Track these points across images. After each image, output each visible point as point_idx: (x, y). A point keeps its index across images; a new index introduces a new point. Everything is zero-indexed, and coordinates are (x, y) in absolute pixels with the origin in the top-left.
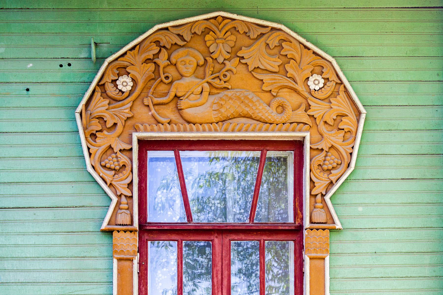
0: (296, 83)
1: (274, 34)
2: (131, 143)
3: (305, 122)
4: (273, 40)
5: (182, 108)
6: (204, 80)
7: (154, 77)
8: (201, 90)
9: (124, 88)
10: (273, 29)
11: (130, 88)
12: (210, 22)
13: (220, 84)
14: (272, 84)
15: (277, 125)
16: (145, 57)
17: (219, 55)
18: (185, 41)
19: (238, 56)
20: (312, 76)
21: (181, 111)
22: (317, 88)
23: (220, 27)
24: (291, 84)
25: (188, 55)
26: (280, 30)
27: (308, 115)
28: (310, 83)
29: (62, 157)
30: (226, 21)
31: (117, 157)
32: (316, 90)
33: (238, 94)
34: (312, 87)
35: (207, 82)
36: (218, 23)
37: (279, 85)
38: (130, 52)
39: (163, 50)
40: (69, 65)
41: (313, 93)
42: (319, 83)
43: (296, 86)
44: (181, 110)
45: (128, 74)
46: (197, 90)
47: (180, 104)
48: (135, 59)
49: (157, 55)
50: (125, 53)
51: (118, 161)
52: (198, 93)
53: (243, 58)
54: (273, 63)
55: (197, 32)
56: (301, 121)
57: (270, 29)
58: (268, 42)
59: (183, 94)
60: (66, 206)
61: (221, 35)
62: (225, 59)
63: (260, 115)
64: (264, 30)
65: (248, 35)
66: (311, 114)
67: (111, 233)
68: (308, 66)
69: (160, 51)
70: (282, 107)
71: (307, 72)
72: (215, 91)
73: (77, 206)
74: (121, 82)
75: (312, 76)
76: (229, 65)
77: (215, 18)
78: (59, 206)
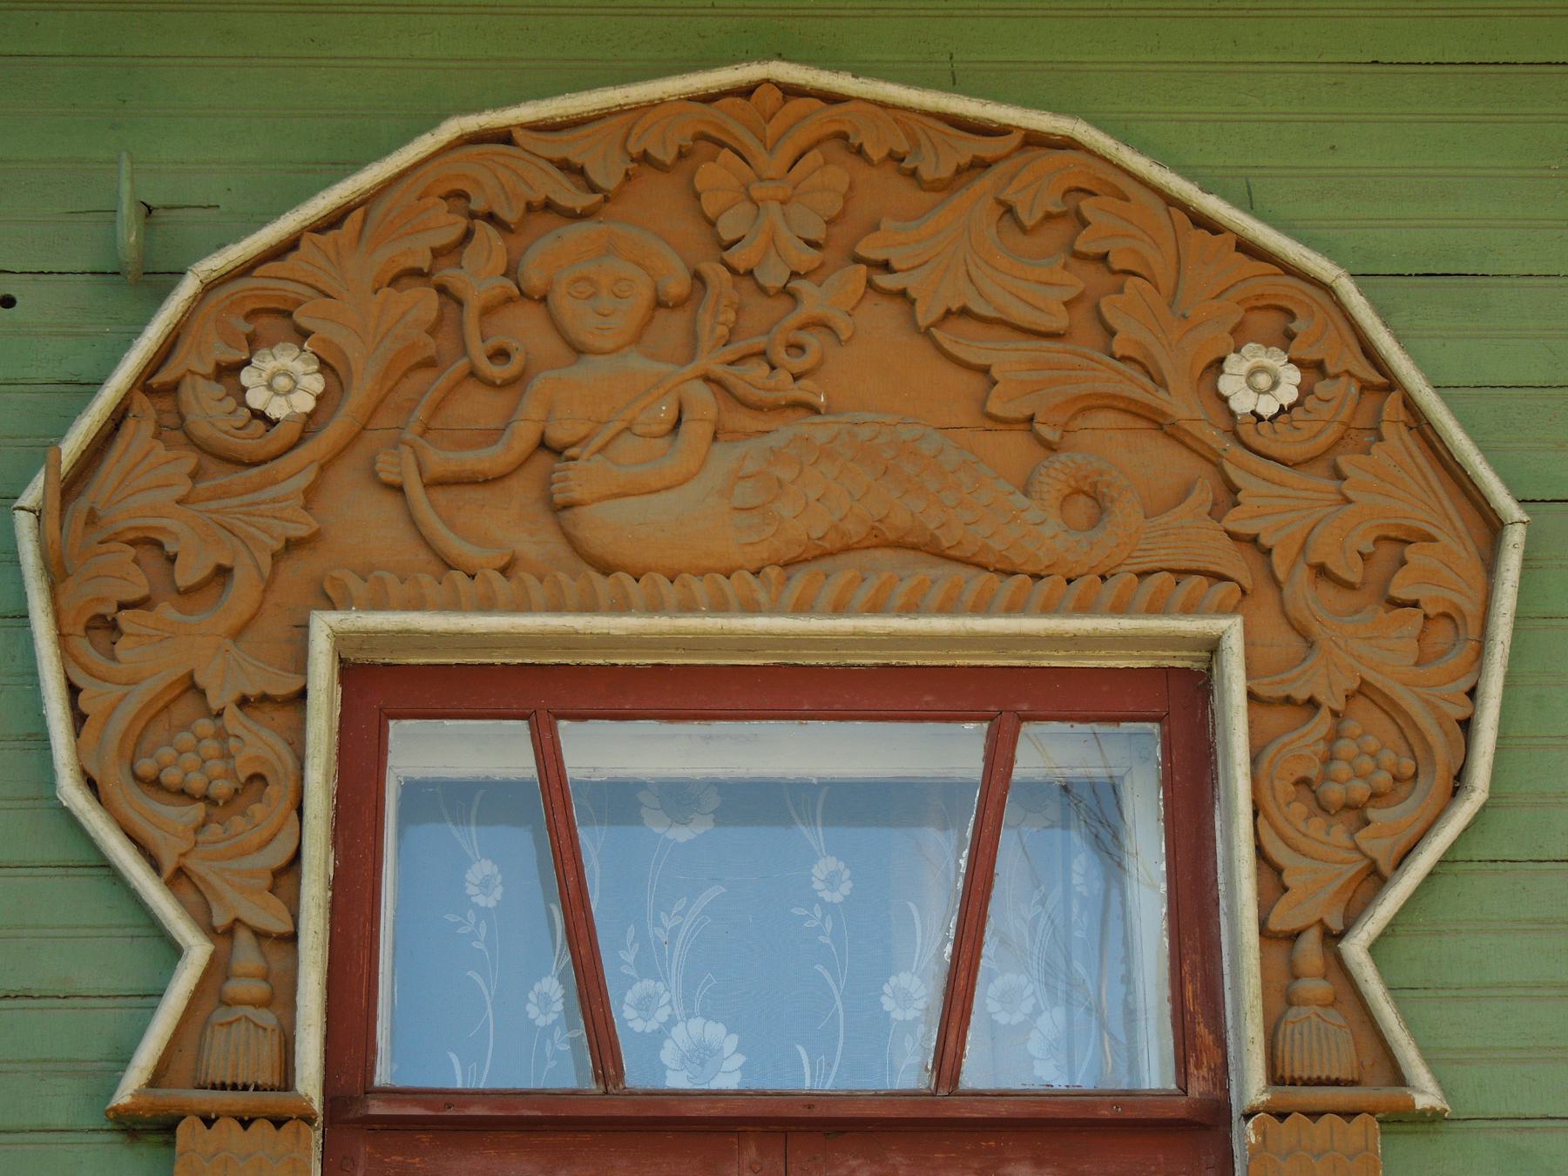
0: (1162, 384)
4: (1035, 190)
5: (577, 494)
6: (689, 370)
9: (281, 401)
10: (1034, 140)
18: (593, 188)
19: (858, 260)
20: (1237, 351)
21: (566, 514)
22: (1268, 407)
24: (1135, 387)
26: (1069, 144)
27: (1226, 531)
30: (798, 105)
31: (222, 735)
32: (1260, 418)
34: (1242, 403)
35: (707, 379)
37: (1084, 389)
41: (1247, 431)
42: (1275, 384)
43: (1159, 399)
44: (567, 506)
50: (289, 246)
51: (226, 755)
52: (656, 429)
53: (886, 266)
54: (1035, 287)
55: (656, 152)
56: (1194, 565)
57: (1014, 140)
58: (1009, 195)
59: (582, 430)
61: (773, 164)
66: (1247, 528)
69: (468, 235)
72: (745, 420)
75: (1237, 351)
77: (746, 91)
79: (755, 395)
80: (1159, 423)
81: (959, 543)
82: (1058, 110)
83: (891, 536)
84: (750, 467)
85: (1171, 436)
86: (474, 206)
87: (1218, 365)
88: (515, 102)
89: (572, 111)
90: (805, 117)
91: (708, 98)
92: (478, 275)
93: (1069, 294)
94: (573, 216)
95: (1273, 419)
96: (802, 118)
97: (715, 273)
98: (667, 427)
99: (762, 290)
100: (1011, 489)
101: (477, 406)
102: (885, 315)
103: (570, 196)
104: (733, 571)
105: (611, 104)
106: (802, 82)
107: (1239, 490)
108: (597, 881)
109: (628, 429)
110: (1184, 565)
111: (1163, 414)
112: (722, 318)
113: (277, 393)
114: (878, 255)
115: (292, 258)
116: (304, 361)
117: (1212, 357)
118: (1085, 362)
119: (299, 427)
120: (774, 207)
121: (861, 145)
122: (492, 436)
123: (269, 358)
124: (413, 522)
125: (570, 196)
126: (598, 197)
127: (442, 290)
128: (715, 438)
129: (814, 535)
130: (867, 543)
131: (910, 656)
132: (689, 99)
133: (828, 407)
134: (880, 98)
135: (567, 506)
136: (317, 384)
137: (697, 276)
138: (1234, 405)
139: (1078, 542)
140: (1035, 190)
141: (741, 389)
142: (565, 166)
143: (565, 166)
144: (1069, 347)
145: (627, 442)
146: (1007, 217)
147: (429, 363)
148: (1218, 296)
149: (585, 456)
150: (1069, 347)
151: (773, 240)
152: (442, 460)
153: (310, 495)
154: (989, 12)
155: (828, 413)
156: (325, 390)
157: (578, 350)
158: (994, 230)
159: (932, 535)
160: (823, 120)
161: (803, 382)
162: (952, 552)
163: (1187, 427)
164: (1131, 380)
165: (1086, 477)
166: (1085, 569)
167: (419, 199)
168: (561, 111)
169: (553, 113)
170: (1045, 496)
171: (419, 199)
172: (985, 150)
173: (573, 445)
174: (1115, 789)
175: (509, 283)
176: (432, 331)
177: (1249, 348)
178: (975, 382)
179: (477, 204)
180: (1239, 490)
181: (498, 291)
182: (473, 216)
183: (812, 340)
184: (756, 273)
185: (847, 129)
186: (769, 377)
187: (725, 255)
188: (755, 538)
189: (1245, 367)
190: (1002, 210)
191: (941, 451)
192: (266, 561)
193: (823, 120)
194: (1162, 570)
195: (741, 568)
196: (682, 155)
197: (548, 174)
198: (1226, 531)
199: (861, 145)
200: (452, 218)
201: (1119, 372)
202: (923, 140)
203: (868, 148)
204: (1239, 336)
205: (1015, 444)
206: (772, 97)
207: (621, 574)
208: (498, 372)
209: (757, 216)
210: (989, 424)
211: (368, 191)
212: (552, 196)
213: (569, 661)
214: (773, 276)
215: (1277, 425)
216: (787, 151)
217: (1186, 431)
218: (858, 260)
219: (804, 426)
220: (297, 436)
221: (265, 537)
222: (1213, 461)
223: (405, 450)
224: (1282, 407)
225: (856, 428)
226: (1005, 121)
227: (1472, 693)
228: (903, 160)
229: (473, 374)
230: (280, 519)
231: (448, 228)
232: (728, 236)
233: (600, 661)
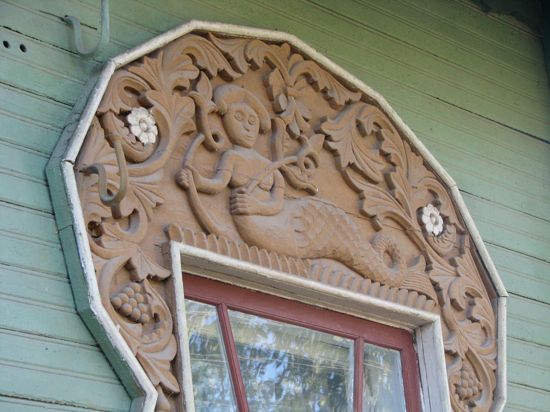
2: (167, 263)
5: (248, 210)
10: (366, 99)
21: (240, 217)
26: (375, 103)
29: (20, 266)
31: (144, 291)
35: (281, 170)
38: (149, 59)
40: (23, 48)
41: (430, 239)
44: (241, 214)
47: (243, 202)
50: (139, 61)
51: (146, 302)
60: (36, 396)
63: (366, 261)
66: (436, 279)
73: (59, 399)
78: (21, 392)
82: (376, 89)
85: (407, 235)
108: (505, 366)
110: (421, 291)
111: (410, 226)
131: (334, 307)
132: (261, 40)
135: (241, 214)
143: (226, 56)
159: (352, 258)
162: (356, 267)
165: (391, 246)
170: (381, 251)
174: (131, 398)
185: (311, 73)
206: (286, 49)
210: (360, 216)
213: (231, 283)
217: (416, 235)
227: (496, 360)
233: (241, 286)
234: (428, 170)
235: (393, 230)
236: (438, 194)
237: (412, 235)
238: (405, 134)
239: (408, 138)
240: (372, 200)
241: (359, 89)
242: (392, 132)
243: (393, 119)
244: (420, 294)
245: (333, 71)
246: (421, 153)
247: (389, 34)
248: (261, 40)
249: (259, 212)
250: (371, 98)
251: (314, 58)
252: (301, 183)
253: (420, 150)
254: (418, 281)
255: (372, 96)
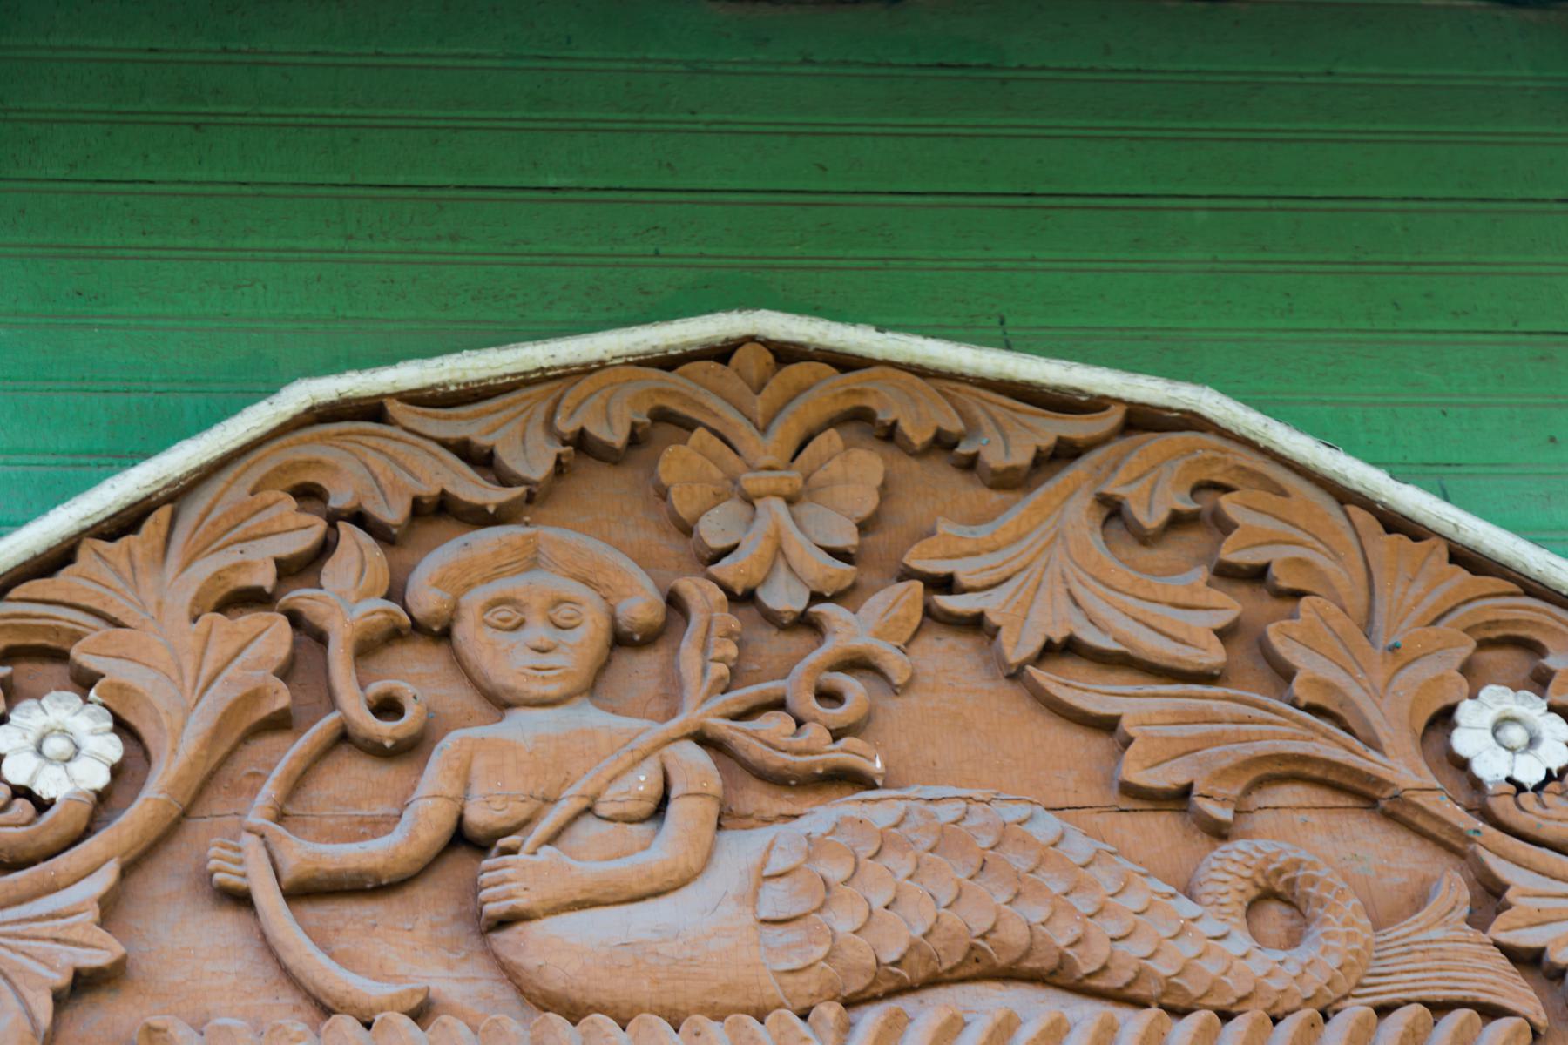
0: (1373, 743)
1: (1133, 458)
3: (1484, 998)
4: (1154, 483)
6: (673, 726)
7: (282, 700)
8: (657, 789)
9: (55, 772)
10: (1142, 420)
11: (101, 779)
12: (684, 375)
13: (801, 742)
14: (1190, 750)
15: (1226, 1016)
16: (218, 576)
17: (772, 567)
18: (505, 480)
19: (907, 574)
20: (1473, 695)
22: (1530, 773)
23: (760, 405)
24: (1329, 747)
25: (532, 561)
26: (1192, 422)
27: (1497, 945)
28: (1470, 738)
30: (797, 372)
32: (1521, 788)
33: (947, 813)
34: (1491, 766)
35: (703, 739)
36: (749, 383)
37: (1247, 751)
38: (102, 545)
39: (351, 537)
41: (1503, 807)
42: (1533, 742)
43: (1371, 762)
44: (504, 922)
45: (84, 682)
46: (621, 786)
48: (136, 586)
49: (302, 568)
52: (632, 808)
53: (946, 584)
54: (1179, 612)
55: (599, 431)
56: (1457, 995)
57: (1115, 416)
58: (1113, 488)
59: (521, 811)
61: (770, 447)
62: (816, 597)
64: (1077, 428)
65: (964, 449)
66: (1527, 938)
67: (351, 731)
68: (1432, 631)
69: (325, 548)
70: (1268, 895)
71: (1436, 670)
72: (757, 799)
74: (32, 738)
75: (1473, 695)
76: (848, 629)
77: (722, 353)
79: (778, 760)
80: (1363, 794)
81: (1105, 968)
83: (1002, 960)
84: (778, 863)
85: (1390, 817)
86: (334, 503)
87: (1445, 718)
88: (391, 360)
89: (473, 375)
90: (807, 389)
91: (668, 362)
92: (347, 597)
93: (1222, 619)
94: (480, 518)
95: (1538, 788)
96: (802, 389)
97: (701, 594)
98: (649, 806)
99: (771, 618)
100: (1172, 890)
101: (353, 780)
102: (945, 656)
103: (473, 489)
104: (767, 1013)
105: (529, 366)
106: (803, 339)
107: (1505, 887)
109: (589, 810)
110: (1441, 994)
111: (1380, 782)
112: (718, 653)
113: (50, 760)
114: (940, 567)
115: (65, 576)
116: (92, 716)
117: (1438, 704)
118: (1258, 713)
119: (86, 808)
120: (779, 505)
121: (895, 424)
122: (380, 826)
123: (38, 712)
124: (268, 948)
125: (473, 489)
126: (518, 491)
127: (295, 619)
128: (719, 826)
129: (890, 956)
130: (962, 972)
132: (639, 364)
133: (885, 776)
134: (918, 361)
135: (504, 922)
136: (114, 749)
137: (675, 603)
138: (1480, 769)
139: (1282, 963)
140: (1154, 483)
141: (756, 752)
142: (465, 451)
143: (465, 451)
144: (1231, 692)
145: (589, 829)
146: (1116, 525)
147: (281, 723)
148: (1435, 622)
149: (529, 844)
150: (1231, 692)
151: (779, 550)
152: (308, 854)
153: (110, 909)
154: (1048, 265)
155: (885, 787)
156: (124, 758)
157: (500, 703)
158: (1100, 538)
160: (831, 392)
161: (844, 742)
163: (1418, 800)
164: (1327, 736)
165: (1279, 872)
166: (1297, 1002)
167: (253, 493)
168: (458, 376)
169: (446, 377)
171: (253, 493)
172: (1072, 437)
173: (508, 832)
175: (395, 608)
176: (286, 672)
177: (1489, 692)
178: (1098, 745)
179: (340, 499)
180: (1505, 887)
181: (379, 617)
182: (333, 519)
183: (853, 687)
184: (762, 594)
186: (796, 734)
187: (713, 569)
188: (797, 963)
189: (1489, 717)
190: (1105, 512)
191: (1062, 837)
192: (44, 1008)
193: (831, 392)
194: (1408, 1002)
195: (781, 1006)
196: (636, 439)
197: (441, 460)
198: (1497, 945)
199: (895, 424)
200: (306, 518)
201: (1307, 726)
202: (983, 419)
203: (905, 426)
204: (1473, 676)
205: (1160, 827)
206: (752, 361)
207: (598, 1017)
208: (386, 730)
209: (752, 519)
210: (1127, 803)
211: (177, 481)
212: (450, 489)
214: (784, 597)
215: (1546, 798)
216: (787, 430)
217: (1420, 809)
218: (907, 574)
219: (847, 806)
220: (82, 825)
221: (42, 970)
222: (1453, 846)
223: (250, 842)
224: (1549, 771)
225: (931, 807)
226: (1099, 390)
228: (956, 445)
229: (343, 737)
230: (65, 942)
231: (303, 535)
232: (717, 542)
234: (1474, 573)
235: (1314, 818)
236: (1544, 641)
237: (1407, 813)
238: (1343, 482)
239: (1359, 494)
240: (1168, 739)
241: (1105, 397)
242: (1282, 492)
243: (1277, 449)
244: (1439, 1008)
245: (970, 372)
246: (1430, 524)
247: (1318, 192)
248: (639, 364)
249: (579, 897)
250: (1169, 409)
251: (879, 356)
252: (798, 759)
253: (1420, 516)
254: (1437, 964)
255: (1167, 403)
